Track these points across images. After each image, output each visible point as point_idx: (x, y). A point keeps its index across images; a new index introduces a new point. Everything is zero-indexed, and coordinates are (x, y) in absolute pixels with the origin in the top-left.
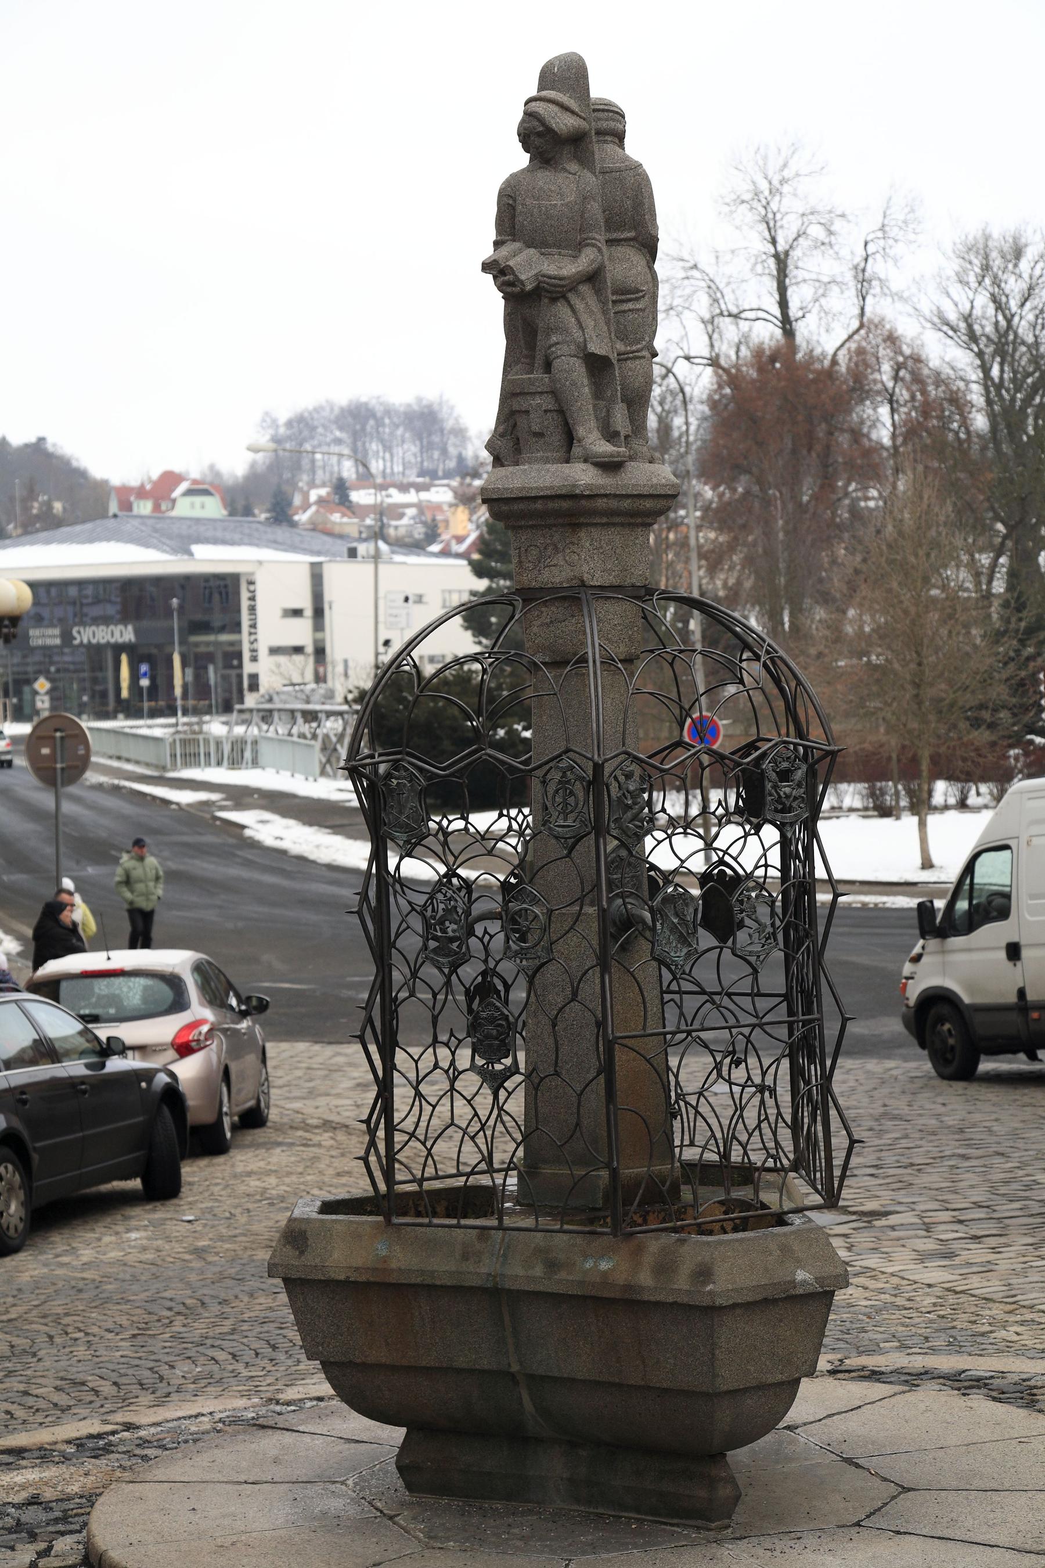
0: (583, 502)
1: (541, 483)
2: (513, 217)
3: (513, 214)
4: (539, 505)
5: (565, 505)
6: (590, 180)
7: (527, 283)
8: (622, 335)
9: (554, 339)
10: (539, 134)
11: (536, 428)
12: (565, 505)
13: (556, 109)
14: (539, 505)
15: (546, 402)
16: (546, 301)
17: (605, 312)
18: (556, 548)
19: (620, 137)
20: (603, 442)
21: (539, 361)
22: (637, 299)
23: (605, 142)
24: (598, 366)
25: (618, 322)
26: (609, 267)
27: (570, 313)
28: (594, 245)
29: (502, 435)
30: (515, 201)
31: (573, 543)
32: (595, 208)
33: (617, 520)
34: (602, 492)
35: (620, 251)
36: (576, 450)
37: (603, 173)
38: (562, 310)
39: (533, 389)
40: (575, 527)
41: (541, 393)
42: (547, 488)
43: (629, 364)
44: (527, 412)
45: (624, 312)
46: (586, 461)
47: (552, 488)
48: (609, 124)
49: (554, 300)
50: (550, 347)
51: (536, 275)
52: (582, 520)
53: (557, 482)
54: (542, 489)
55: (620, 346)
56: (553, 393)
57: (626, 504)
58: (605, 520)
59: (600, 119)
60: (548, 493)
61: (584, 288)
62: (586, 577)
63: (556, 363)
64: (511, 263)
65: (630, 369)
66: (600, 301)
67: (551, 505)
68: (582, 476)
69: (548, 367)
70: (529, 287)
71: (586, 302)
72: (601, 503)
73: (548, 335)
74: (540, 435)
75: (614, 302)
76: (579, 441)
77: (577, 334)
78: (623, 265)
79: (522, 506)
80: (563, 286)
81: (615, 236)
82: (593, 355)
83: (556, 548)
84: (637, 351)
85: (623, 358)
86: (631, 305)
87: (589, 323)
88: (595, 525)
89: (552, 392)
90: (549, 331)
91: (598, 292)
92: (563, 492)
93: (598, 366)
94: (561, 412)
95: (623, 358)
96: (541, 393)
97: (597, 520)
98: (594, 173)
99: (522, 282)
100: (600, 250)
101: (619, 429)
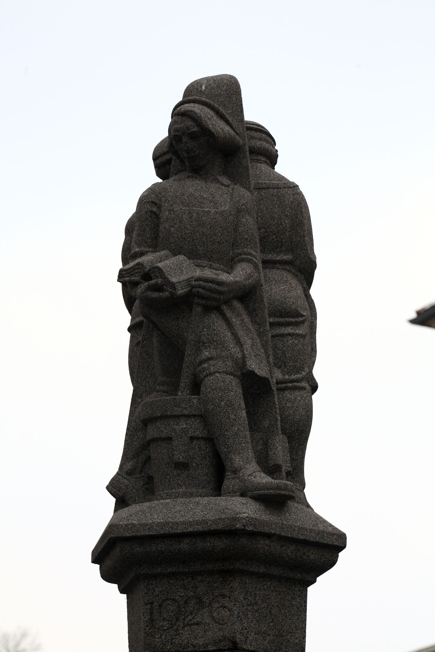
0: (244, 541)
1: (189, 517)
2: (156, 226)
3: (148, 228)
4: (185, 545)
5: (220, 544)
6: (244, 195)
7: (179, 287)
8: (280, 362)
9: (206, 354)
10: (193, 136)
11: (180, 457)
12: (220, 544)
13: (212, 113)
14: (185, 545)
15: (195, 428)
16: (199, 309)
17: (260, 335)
18: (200, 602)
19: (272, 159)
20: (263, 475)
21: (185, 380)
22: (297, 324)
23: (258, 161)
24: (255, 389)
25: (275, 348)
26: (265, 287)
27: (225, 327)
28: (249, 261)
29: (130, 473)
30: (159, 207)
31: (224, 596)
32: (249, 222)
33: (276, 571)
34: (266, 530)
35: (276, 274)
36: (229, 482)
37: (259, 188)
38: (216, 322)
39: (177, 411)
40: (227, 574)
41: (188, 416)
42: (198, 523)
43: (287, 394)
44: (169, 439)
45: (283, 335)
46: (243, 495)
47: (205, 522)
48: (261, 146)
49: (208, 309)
50: (201, 363)
51: (188, 280)
52: (238, 565)
53: (211, 516)
54: (191, 524)
55: (278, 375)
56: (203, 417)
57: (290, 551)
58: (262, 569)
59: (253, 138)
60: (200, 528)
61: (237, 304)
62: (239, 638)
63: (209, 381)
64: (160, 265)
65: (289, 400)
66: (254, 322)
67: (201, 545)
68: (246, 510)
69: (196, 387)
70: (180, 292)
71: (240, 318)
72: (262, 545)
73: (198, 350)
74: (183, 466)
75: (272, 325)
76: (235, 471)
77: (235, 350)
78: (279, 287)
79: (162, 546)
80: (221, 293)
81: (269, 257)
82: (252, 373)
83: (200, 602)
84: (297, 381)
85: (284, 386)
86: (289, 330)
87: (247, 342)
88: (252, 574)
89: (201, 416)
90: (200, 344)
91: (251, 313)
92: (220, 526)
93: (255, 389)
94: (210, 440)
95: (284, 386)
96: (188, 416)
97: (254, 568)
98: (248, 189)
99: (173, 286)
100: (256, 266)
101: (281, 463)
